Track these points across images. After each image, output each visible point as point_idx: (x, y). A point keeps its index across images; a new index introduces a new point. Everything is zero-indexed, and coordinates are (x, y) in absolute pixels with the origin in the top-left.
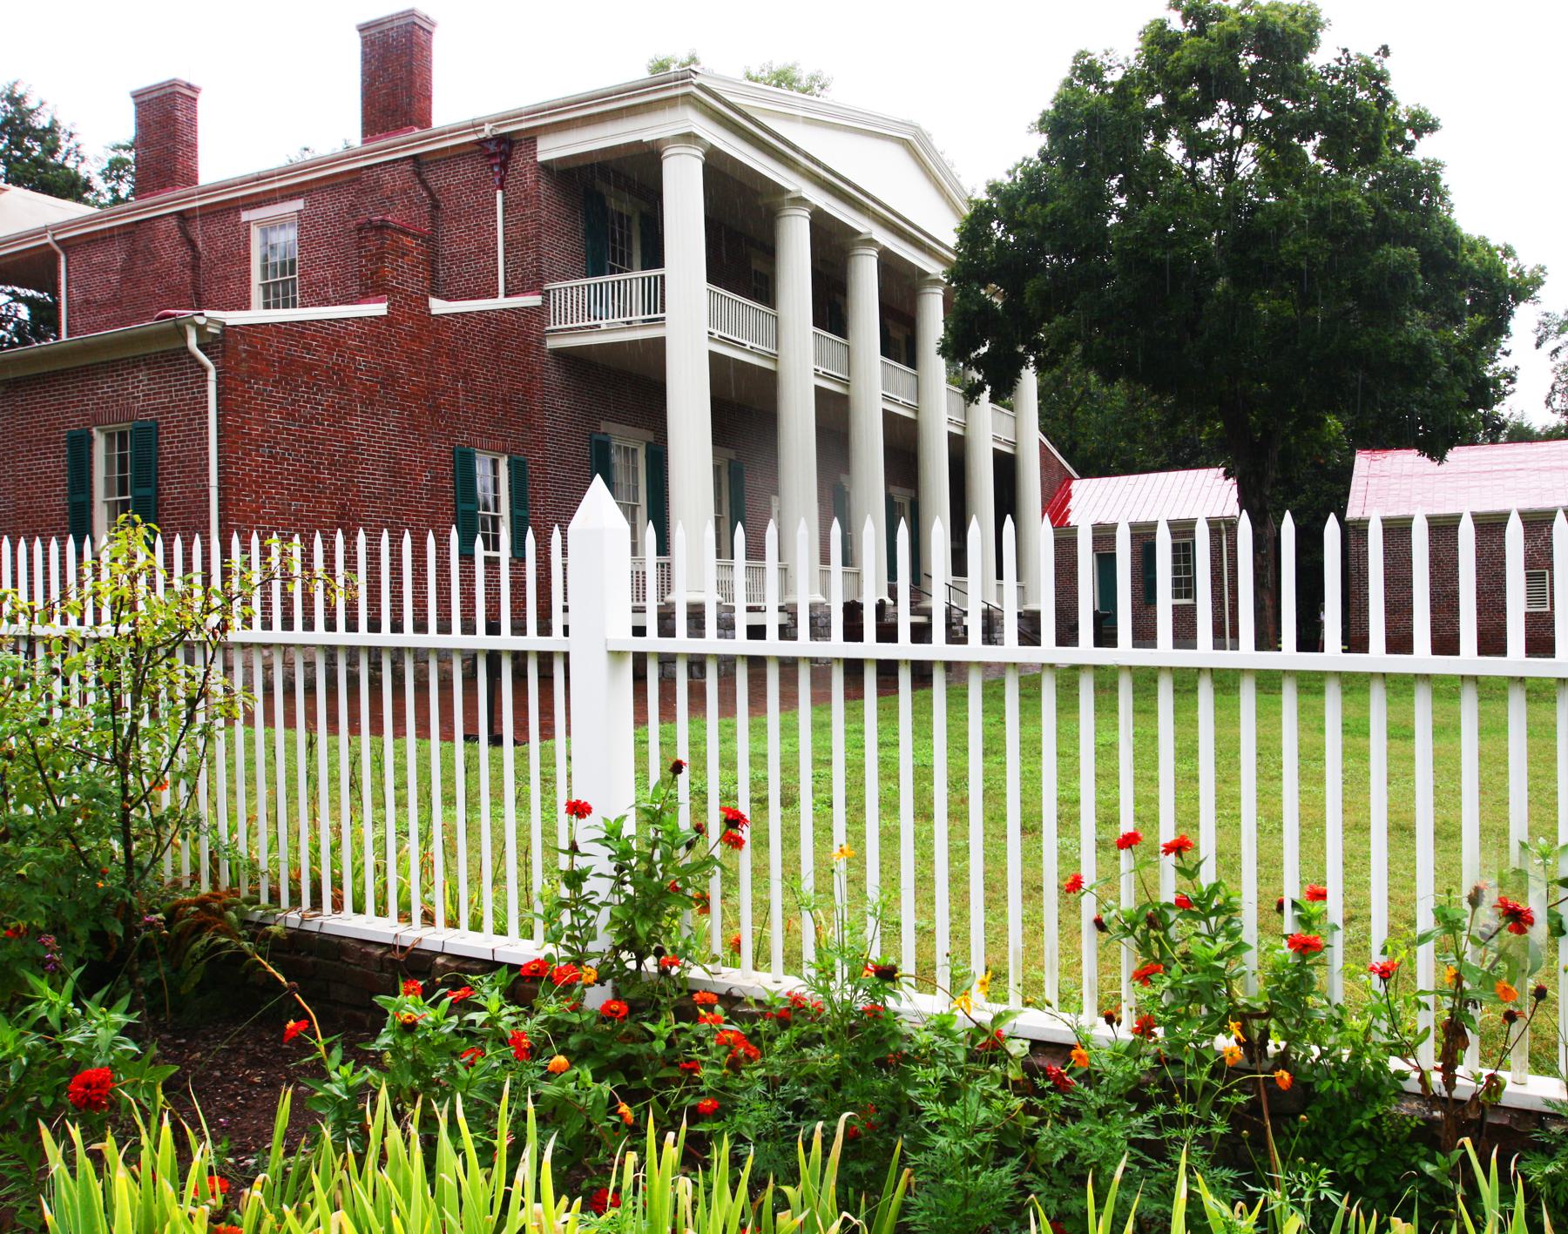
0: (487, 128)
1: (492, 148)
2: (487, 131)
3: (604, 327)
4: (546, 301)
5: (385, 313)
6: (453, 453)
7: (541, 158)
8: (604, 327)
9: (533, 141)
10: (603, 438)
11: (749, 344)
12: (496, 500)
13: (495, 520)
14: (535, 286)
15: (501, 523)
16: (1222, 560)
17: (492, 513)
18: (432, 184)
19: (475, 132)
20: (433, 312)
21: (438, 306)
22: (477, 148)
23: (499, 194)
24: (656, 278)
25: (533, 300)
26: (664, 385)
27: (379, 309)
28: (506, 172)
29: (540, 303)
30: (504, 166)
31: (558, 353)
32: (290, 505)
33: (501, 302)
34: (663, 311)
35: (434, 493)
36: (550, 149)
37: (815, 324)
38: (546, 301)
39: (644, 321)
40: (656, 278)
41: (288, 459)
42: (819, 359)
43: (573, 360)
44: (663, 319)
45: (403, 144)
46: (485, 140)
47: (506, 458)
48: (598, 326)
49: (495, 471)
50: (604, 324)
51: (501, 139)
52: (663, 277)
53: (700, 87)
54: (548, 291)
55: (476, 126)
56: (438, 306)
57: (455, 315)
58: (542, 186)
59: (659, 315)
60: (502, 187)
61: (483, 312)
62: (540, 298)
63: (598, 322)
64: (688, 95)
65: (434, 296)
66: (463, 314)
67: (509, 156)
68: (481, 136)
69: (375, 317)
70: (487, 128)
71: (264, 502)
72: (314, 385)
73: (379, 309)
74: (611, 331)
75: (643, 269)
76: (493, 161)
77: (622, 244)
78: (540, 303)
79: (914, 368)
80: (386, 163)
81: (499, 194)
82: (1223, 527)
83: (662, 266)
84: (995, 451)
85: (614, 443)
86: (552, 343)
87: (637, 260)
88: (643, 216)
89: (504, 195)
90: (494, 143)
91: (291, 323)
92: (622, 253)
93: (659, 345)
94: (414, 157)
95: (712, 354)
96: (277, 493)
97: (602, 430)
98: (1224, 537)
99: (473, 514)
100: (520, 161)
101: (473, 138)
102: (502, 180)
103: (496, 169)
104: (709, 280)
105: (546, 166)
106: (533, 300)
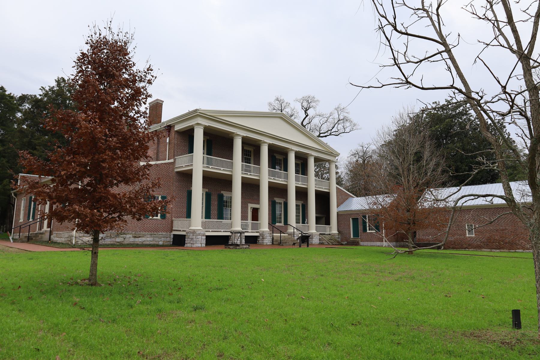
1: (167, 128)
9: (174, 126)
36: (177, 128)
53: (200, 113)
60: (169, 136)
67: (170, 130)
102: (169, 135)
105: (177, 132)
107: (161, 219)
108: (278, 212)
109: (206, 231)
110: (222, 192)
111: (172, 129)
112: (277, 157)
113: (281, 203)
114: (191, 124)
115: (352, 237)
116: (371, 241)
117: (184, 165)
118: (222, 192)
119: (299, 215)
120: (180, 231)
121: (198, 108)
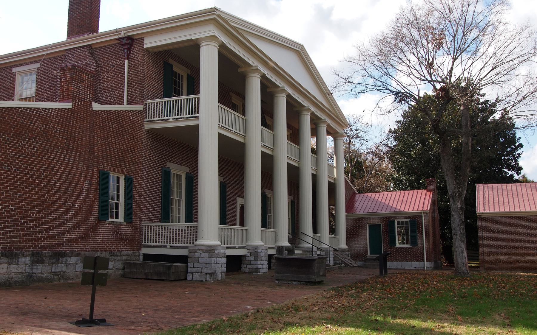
0: (122, 33)
1: (124, 41)
2: (122, 34)
3: (171, 120)
4: (145, 108)
5: (71, 107)
6: (99, 173)
7: (145, 46)
8: (171, 120)
9: (143, 39)
10: (168, 170)
11: (234, 130)
12: (118, 196)
13: (117, 205)
14: (141, 102)
15: (120, 206)
16: (422, 229)
17: (116, 201)
18: (98, 58)
19: (117, 35)
20: (94, 109)
21: (96, 106)
22: (118, 42)
23: (126, 61)
24: (195, 99)
25: (140, 107)
26: (198, 149)
27: (68, 105)
28: (130, 52)
29: (142, 109)
30: (129, 49)
31: (150, 131)
32: (17, 194)
33: (409, 225)
34: (198, 113)
35: (89, 191)
36: (150, 43)
37: (262, 125)
38: (145, 108)
39: (187, 118)
40: (195, 99)
41: (17, 173)
42: (263, 140)
43: (155, 134)
44: (198, 117)
45: (86, 40)
46: (121, 38)
47: (124, 177)
48: (168, 119)
49: (118, 182)
50: (171, 118)
51: (129, 38)
52: (198, 98)
53: (219, 16)
54: (146, 104)
55: (117, 31)
56: (96, 106)
57: (104, 111)
58: (146, 58)
59: (196, 115)
60: (128, 59)
61: (117, 110)
62: (143, 106)
63: (166, 244)
64: (214, 19)
65: (95, 102)
66: (107, 111)
67: (131, 45)
68: (120, 36)
69: (66, 109)
70: (122, 33)
71: (3, 193)
72: (33, 138)
73: (68, 105)
74: (172, 122)
75: (188, 94)
76: (124, 47)
77: (179, 87)
78: (142, 109)
79: (299, 146)
80: (78, 47)
81: (126, 61)
82: (423, 215)
83: (198, 93)
84: (289, 164)
85: (172, 172)
86: (147, 126)
87: (185, 91)
88: (189, 77)
89: (129, 62)
90: (125, 39)
91: (24, 108)
92: (179, 90)
93: (196, 128)
94: (90, 45)
95: (220, 134)
96: (10, 189)
97: (167, 166)
98: (423, 219)
99: (107, 202)
100: (136, 48)
101: (117, 37)
102: (128, 55)
103: (126, 51)
104: (219, 102)
105: (147, 50)
106: (140, 107)
107: (125, 224)
108: (112, 192)
109: (227, 248)
110: (169, 165)
111: (135, 44)
112: (175, 69)
113: (181, 176)
114: (193, 37)
115: (369, 254)
116: (403, 261)
117: (234, 130)
118: (169, 165)
119: (179, 201)
120: (234, 248)
121: (218, 7)
